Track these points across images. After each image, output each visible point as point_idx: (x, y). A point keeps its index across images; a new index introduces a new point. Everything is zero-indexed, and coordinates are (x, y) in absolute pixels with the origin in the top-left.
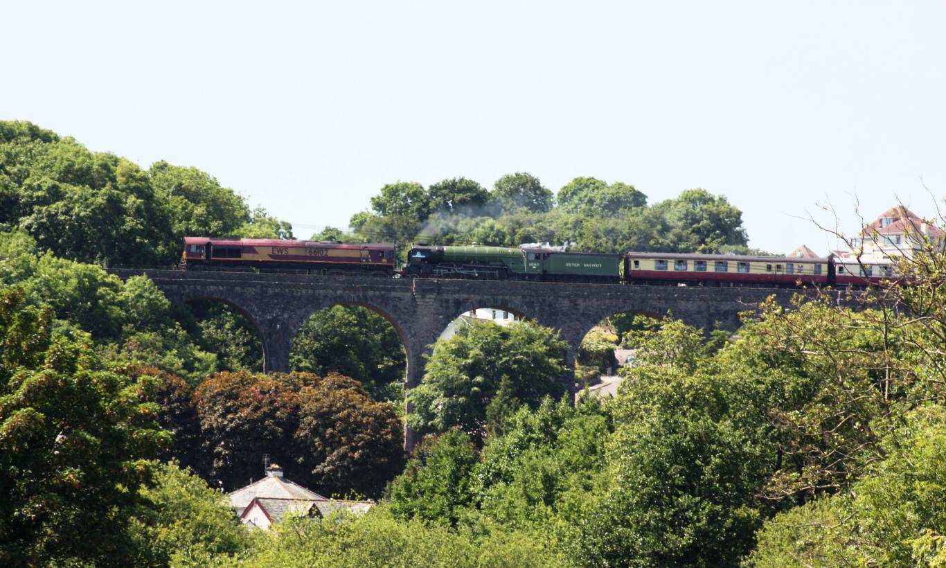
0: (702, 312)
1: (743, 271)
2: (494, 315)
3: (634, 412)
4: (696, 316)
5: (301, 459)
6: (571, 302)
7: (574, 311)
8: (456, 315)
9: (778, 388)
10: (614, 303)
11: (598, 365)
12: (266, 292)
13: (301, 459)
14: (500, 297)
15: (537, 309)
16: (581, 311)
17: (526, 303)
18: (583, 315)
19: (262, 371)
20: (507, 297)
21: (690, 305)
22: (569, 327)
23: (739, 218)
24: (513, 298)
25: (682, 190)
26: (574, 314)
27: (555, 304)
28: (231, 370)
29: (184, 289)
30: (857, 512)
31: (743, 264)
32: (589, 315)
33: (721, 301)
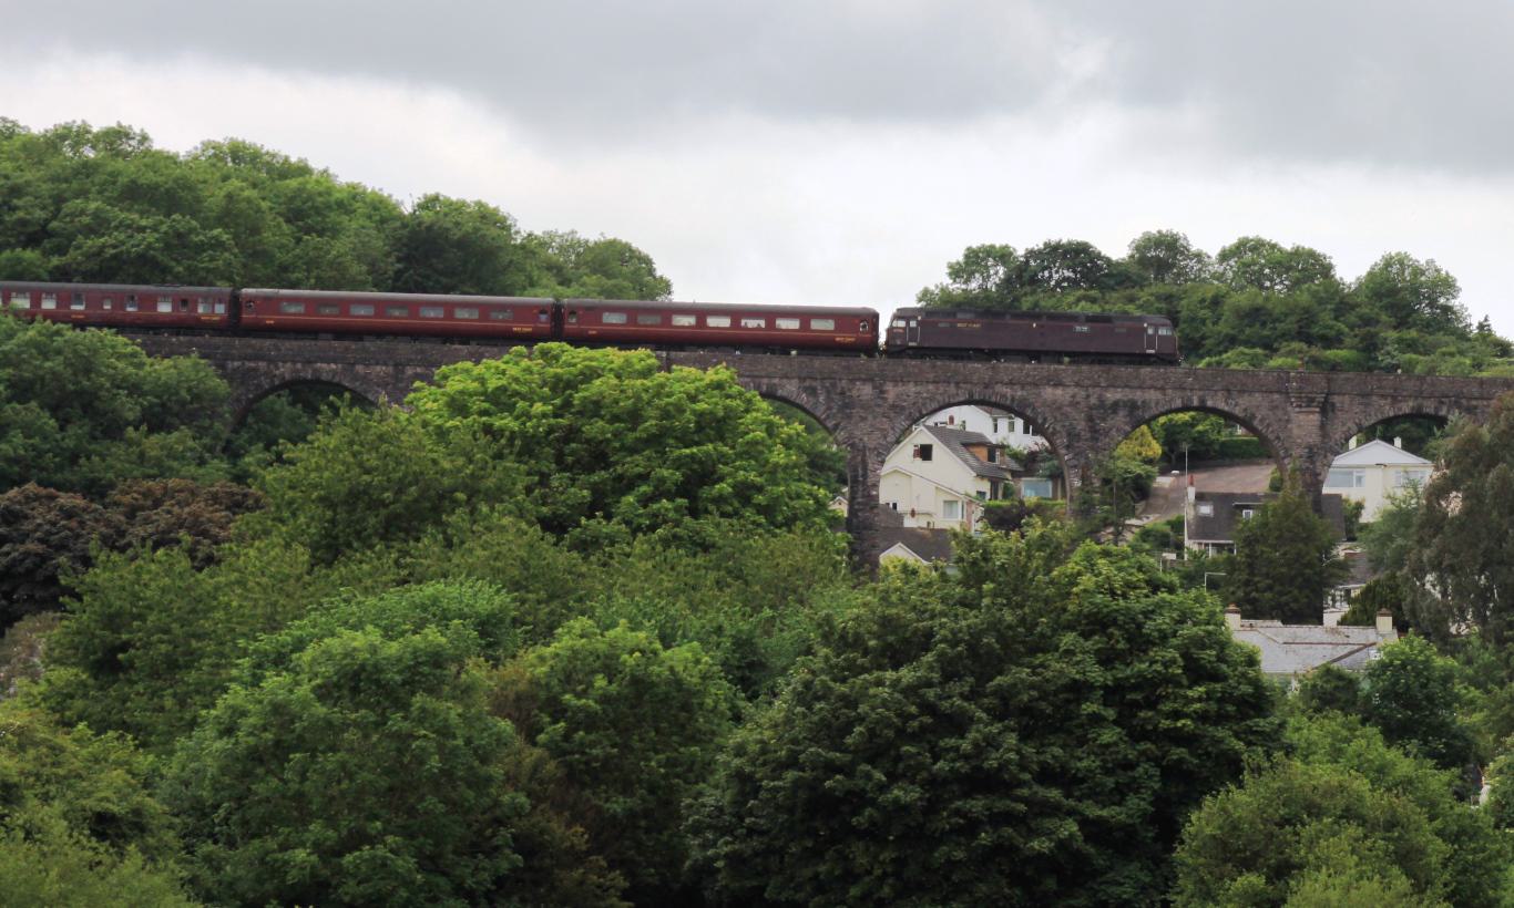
0: (1078, 403)
1: (184, 312)
2: (996, 426)
4: (1069, 409)
6: (874, 388)
9: (402, 460)
10: (941, 390)
11: (251, 442)
12: (403, 372)
14: (765, 381)
15: (821, 399)
16: (890, 401)
17: (806, 389)
18: (893, 407)
20: (776, 381)
21: (1059, 391)
23: (1040, 252)
24: (785, 381)
25: (355, 180)
26: (879, 406)
27: (850, 390)
28: (585, 559)
29: (278, 368)
31: (184, 302)
32: (903, 408)
33: (1108, 386)
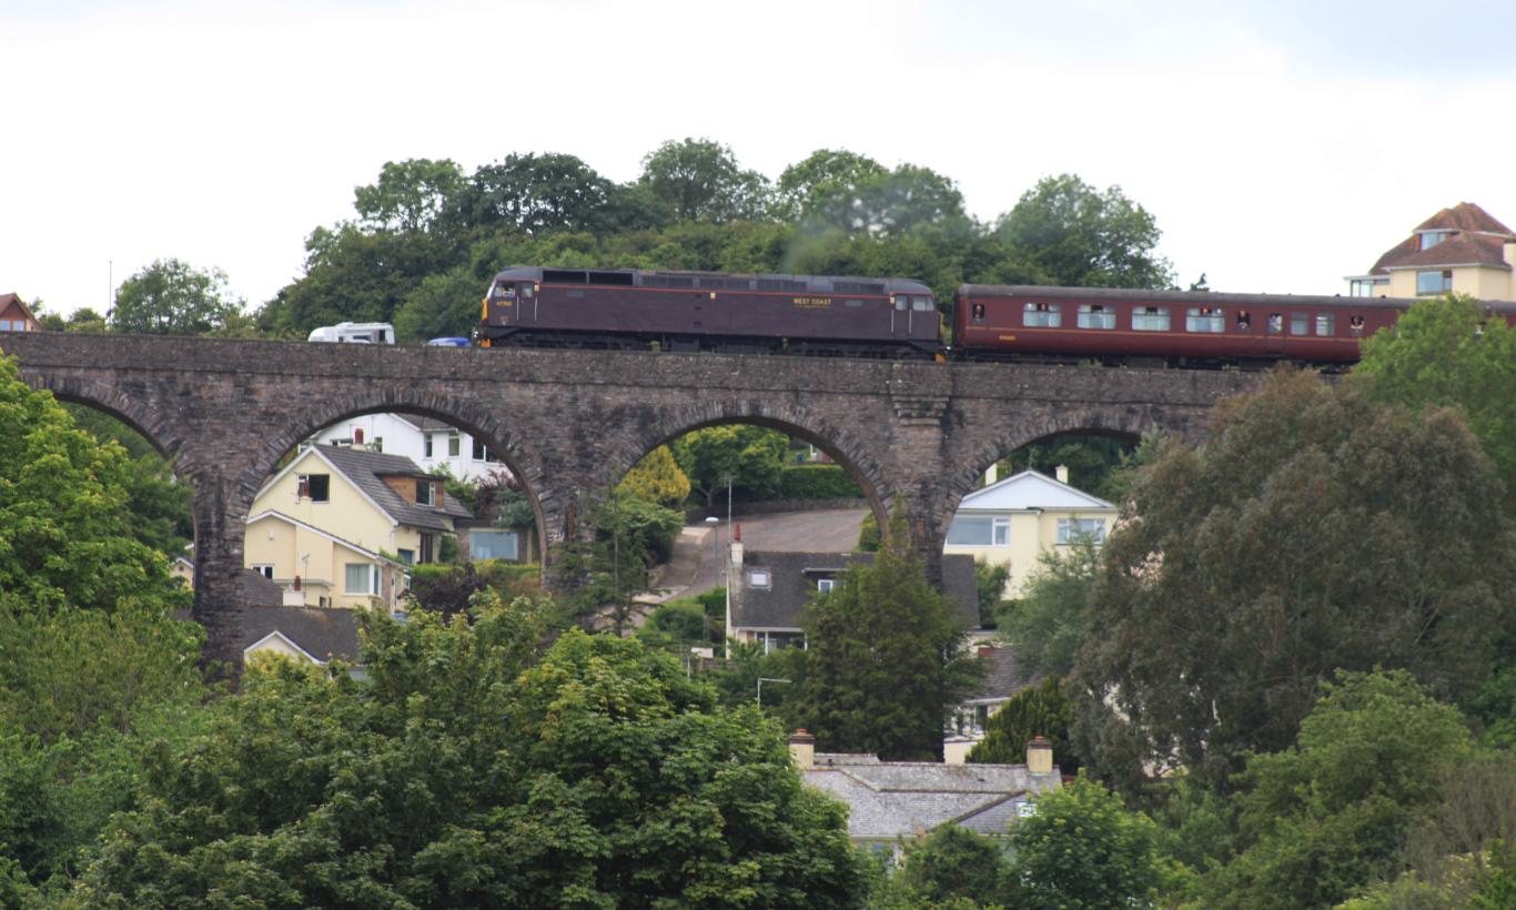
0: (559, 410)
3: (447, 801)
5: (713, 295)
7: (245, 407)
8: (383, 321)
13: (713, 295)
14: (63, 372)
15: (152, 401)
16: (262, 406)
17: (127, 387)
18: (267, 415)
19: (591, 274)
21: (529, 392)
22: (231, 445)
23: (500, 170)
24: (94, 373)
26: (244, 413)
27: (198, 389)
30: (1273, 612)
32: (282, 417)
